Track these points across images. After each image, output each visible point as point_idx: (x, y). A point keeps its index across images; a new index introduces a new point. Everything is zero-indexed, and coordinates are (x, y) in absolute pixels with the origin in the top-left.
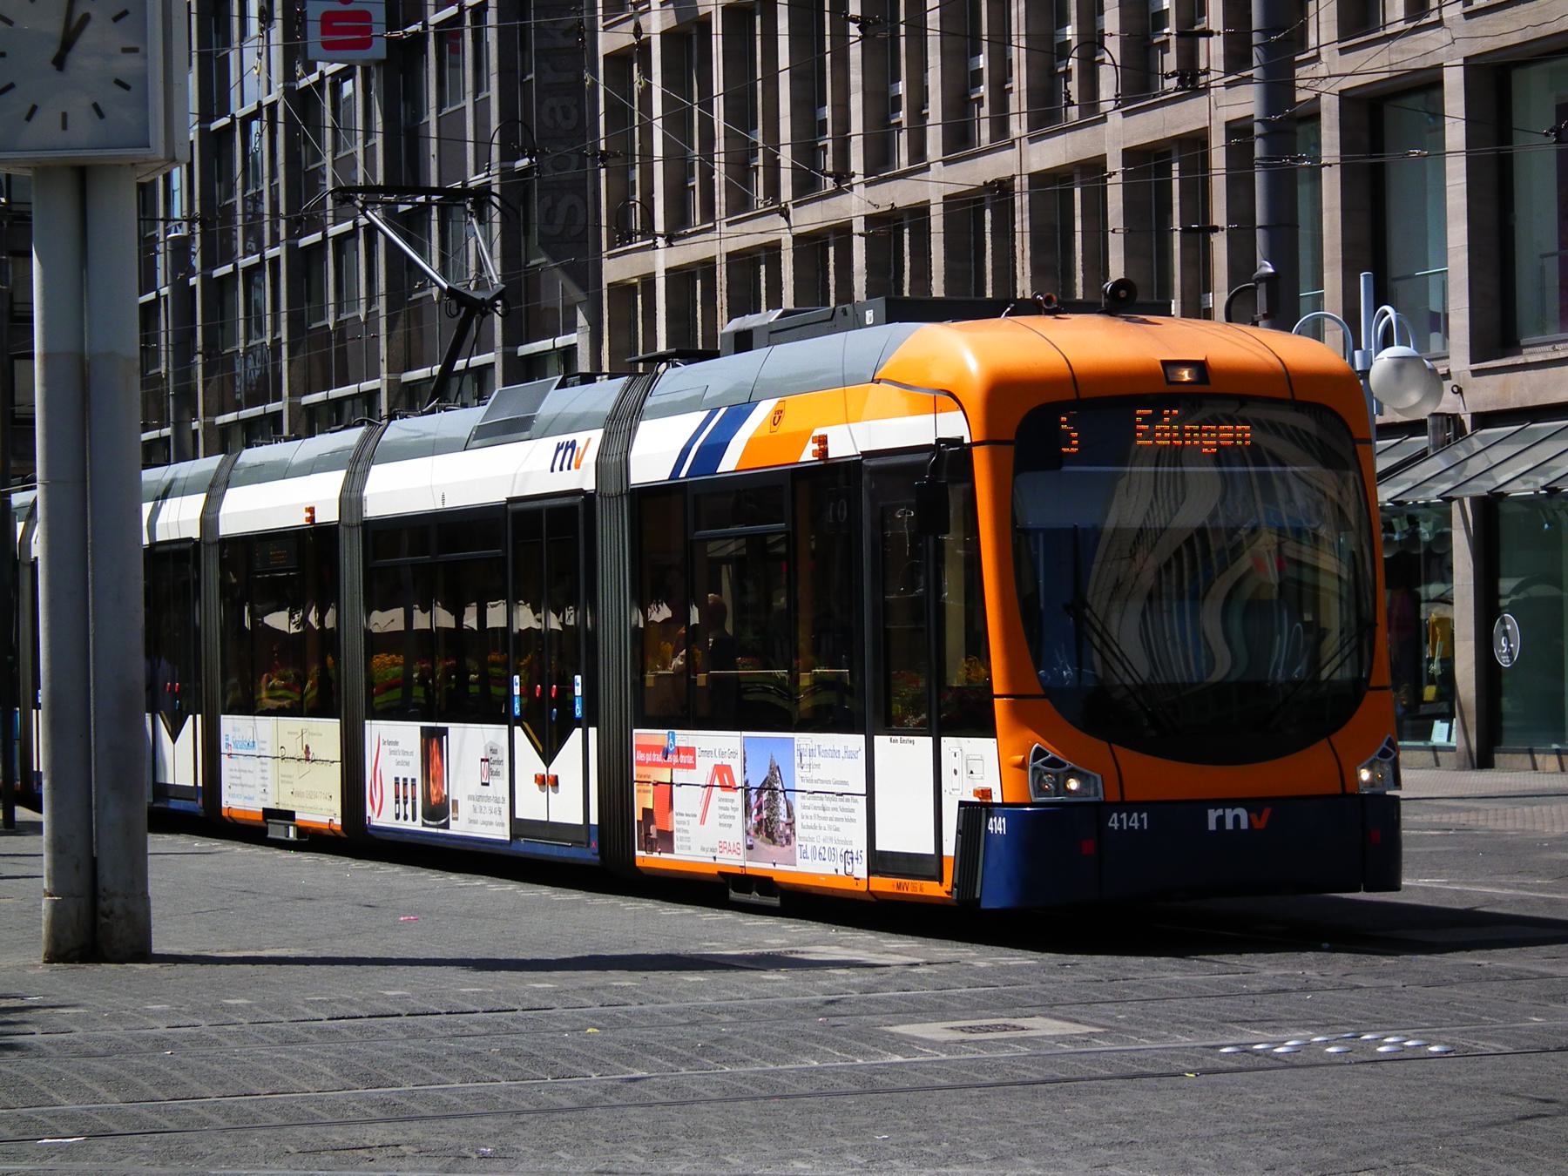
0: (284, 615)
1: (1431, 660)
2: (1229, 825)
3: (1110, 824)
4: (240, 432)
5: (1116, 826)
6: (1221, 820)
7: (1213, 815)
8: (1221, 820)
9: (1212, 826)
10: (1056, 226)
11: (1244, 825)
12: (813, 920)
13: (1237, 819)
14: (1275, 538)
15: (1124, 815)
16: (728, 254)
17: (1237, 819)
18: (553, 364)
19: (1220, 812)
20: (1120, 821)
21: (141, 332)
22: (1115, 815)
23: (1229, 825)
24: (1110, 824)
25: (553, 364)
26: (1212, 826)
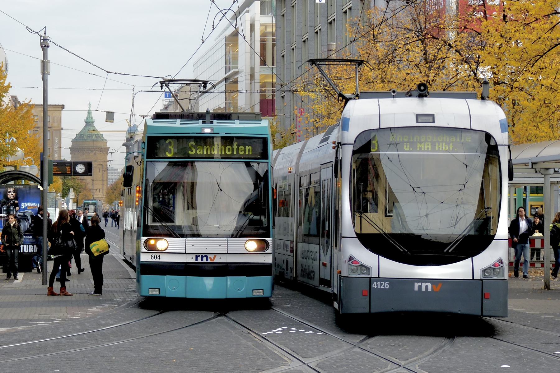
0: (53, 256)
1: (76, 218)
2: (423, 289)
3: (373, 286)
4: (523, 227)
5: (376, 287)
6: (420, 287)
7: (417, 285)
8: (420, 287)
9: (416, 289)
10: (265, 92)
11: (430, 289)
12: (306, 295)
13: (427, 287)
14: (478, 78)
15: (379, 283)
16: (165, 98)
17: (427, 287)
18: (189, 164)
19: (420, 284)
20: (377, 285)
21: (132, 176)
22: (375, 283)
23: (423, 289)
24: (373, 286)
25: (189, 164)
26: (416, 289)
